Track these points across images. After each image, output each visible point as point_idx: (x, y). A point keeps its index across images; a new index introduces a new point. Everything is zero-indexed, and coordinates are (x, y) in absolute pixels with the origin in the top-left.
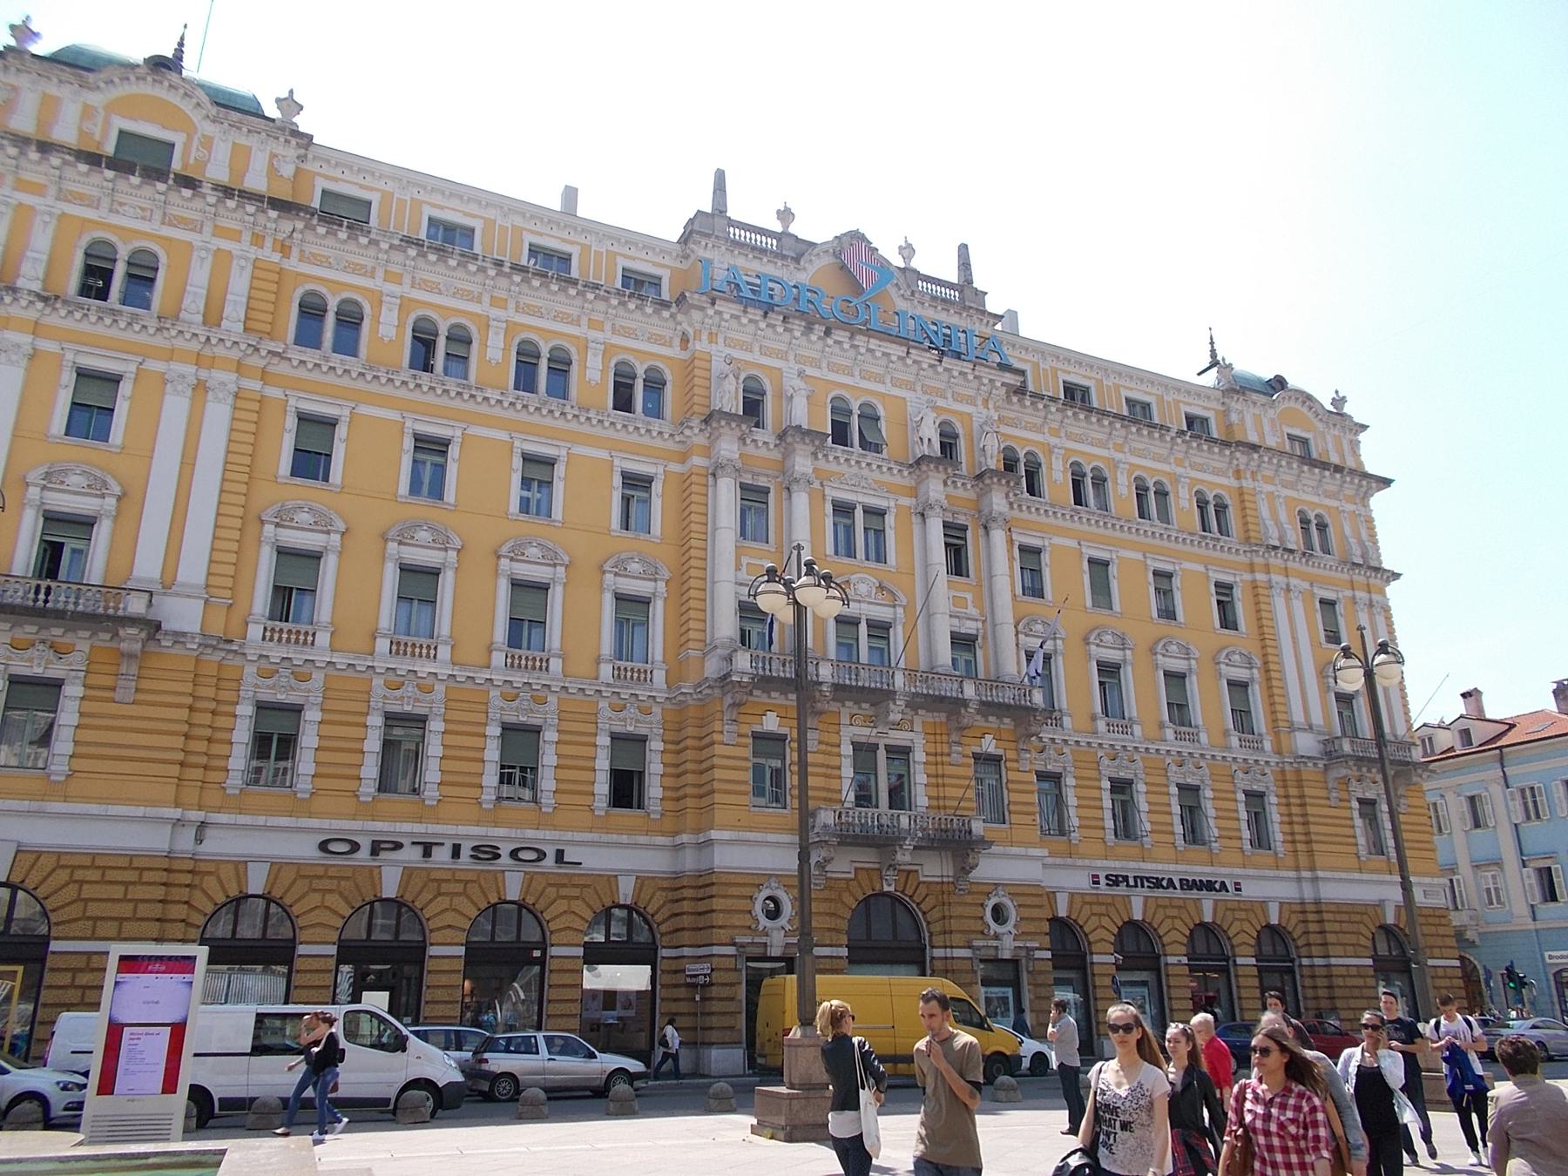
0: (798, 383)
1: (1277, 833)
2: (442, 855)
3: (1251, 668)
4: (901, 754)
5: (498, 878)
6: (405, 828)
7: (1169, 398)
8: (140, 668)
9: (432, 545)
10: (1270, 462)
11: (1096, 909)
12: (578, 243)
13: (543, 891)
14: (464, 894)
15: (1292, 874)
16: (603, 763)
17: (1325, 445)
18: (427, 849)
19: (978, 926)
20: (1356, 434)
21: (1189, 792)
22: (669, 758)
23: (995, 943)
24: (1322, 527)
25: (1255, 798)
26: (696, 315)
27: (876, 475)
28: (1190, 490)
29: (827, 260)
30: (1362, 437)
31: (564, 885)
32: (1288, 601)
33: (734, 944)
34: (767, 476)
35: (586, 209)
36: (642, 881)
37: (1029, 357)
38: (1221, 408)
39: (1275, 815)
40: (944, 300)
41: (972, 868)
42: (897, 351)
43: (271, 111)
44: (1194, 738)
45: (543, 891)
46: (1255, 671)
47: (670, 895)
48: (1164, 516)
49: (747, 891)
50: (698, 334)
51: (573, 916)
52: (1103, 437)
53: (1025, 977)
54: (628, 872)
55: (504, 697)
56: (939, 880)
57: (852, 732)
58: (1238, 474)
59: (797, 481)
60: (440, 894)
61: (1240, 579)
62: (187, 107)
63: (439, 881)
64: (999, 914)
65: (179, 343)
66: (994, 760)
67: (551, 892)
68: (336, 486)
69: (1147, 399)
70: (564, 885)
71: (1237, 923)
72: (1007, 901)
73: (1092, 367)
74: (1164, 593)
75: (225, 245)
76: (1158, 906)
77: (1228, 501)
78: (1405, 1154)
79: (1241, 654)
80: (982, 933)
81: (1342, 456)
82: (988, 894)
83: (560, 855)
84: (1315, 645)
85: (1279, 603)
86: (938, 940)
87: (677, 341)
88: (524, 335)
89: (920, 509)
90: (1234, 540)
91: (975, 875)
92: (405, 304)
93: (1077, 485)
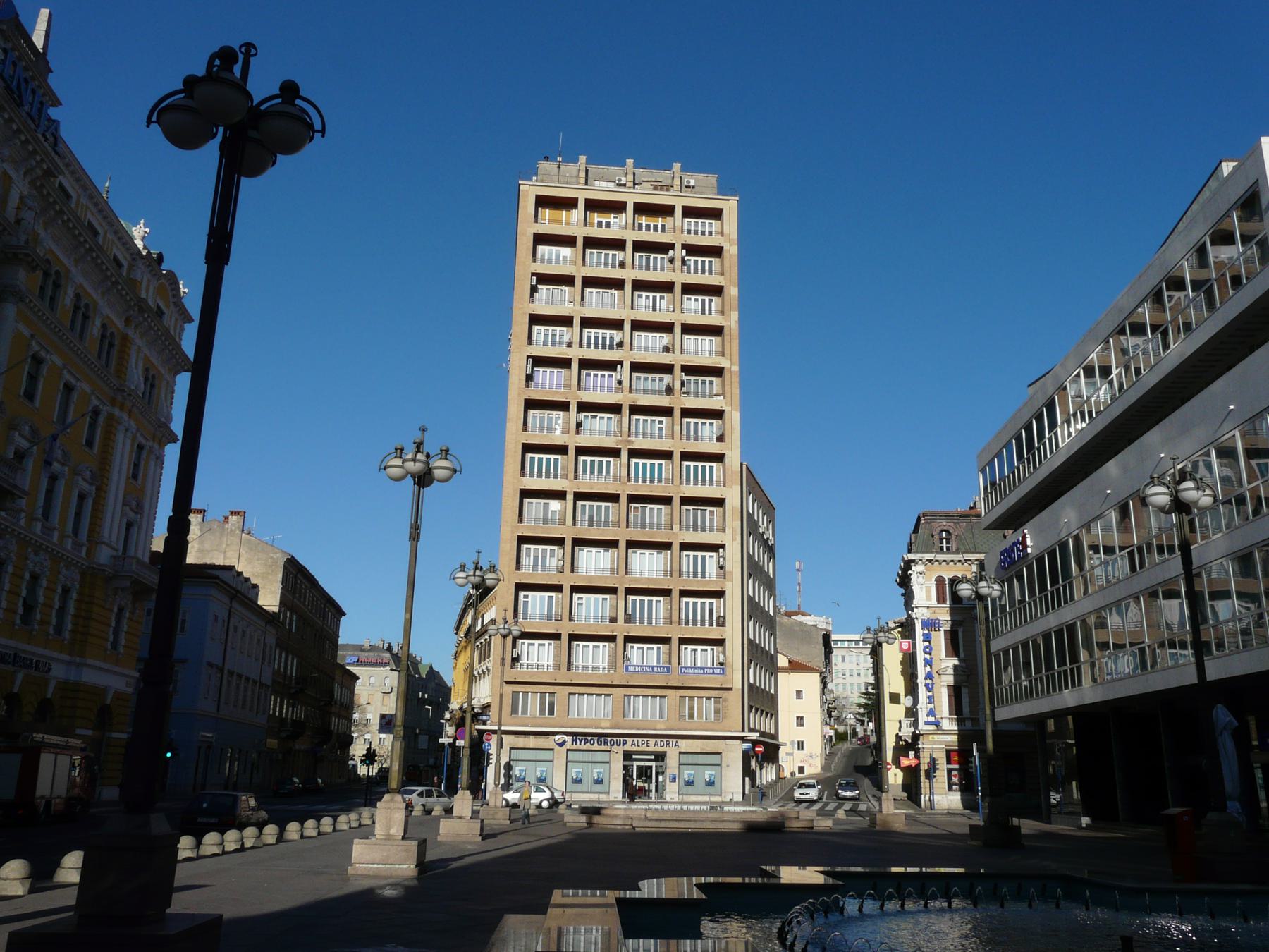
15: (66, 657)
20: (185, 323)
81: (147, 296)
85: (120, 437)
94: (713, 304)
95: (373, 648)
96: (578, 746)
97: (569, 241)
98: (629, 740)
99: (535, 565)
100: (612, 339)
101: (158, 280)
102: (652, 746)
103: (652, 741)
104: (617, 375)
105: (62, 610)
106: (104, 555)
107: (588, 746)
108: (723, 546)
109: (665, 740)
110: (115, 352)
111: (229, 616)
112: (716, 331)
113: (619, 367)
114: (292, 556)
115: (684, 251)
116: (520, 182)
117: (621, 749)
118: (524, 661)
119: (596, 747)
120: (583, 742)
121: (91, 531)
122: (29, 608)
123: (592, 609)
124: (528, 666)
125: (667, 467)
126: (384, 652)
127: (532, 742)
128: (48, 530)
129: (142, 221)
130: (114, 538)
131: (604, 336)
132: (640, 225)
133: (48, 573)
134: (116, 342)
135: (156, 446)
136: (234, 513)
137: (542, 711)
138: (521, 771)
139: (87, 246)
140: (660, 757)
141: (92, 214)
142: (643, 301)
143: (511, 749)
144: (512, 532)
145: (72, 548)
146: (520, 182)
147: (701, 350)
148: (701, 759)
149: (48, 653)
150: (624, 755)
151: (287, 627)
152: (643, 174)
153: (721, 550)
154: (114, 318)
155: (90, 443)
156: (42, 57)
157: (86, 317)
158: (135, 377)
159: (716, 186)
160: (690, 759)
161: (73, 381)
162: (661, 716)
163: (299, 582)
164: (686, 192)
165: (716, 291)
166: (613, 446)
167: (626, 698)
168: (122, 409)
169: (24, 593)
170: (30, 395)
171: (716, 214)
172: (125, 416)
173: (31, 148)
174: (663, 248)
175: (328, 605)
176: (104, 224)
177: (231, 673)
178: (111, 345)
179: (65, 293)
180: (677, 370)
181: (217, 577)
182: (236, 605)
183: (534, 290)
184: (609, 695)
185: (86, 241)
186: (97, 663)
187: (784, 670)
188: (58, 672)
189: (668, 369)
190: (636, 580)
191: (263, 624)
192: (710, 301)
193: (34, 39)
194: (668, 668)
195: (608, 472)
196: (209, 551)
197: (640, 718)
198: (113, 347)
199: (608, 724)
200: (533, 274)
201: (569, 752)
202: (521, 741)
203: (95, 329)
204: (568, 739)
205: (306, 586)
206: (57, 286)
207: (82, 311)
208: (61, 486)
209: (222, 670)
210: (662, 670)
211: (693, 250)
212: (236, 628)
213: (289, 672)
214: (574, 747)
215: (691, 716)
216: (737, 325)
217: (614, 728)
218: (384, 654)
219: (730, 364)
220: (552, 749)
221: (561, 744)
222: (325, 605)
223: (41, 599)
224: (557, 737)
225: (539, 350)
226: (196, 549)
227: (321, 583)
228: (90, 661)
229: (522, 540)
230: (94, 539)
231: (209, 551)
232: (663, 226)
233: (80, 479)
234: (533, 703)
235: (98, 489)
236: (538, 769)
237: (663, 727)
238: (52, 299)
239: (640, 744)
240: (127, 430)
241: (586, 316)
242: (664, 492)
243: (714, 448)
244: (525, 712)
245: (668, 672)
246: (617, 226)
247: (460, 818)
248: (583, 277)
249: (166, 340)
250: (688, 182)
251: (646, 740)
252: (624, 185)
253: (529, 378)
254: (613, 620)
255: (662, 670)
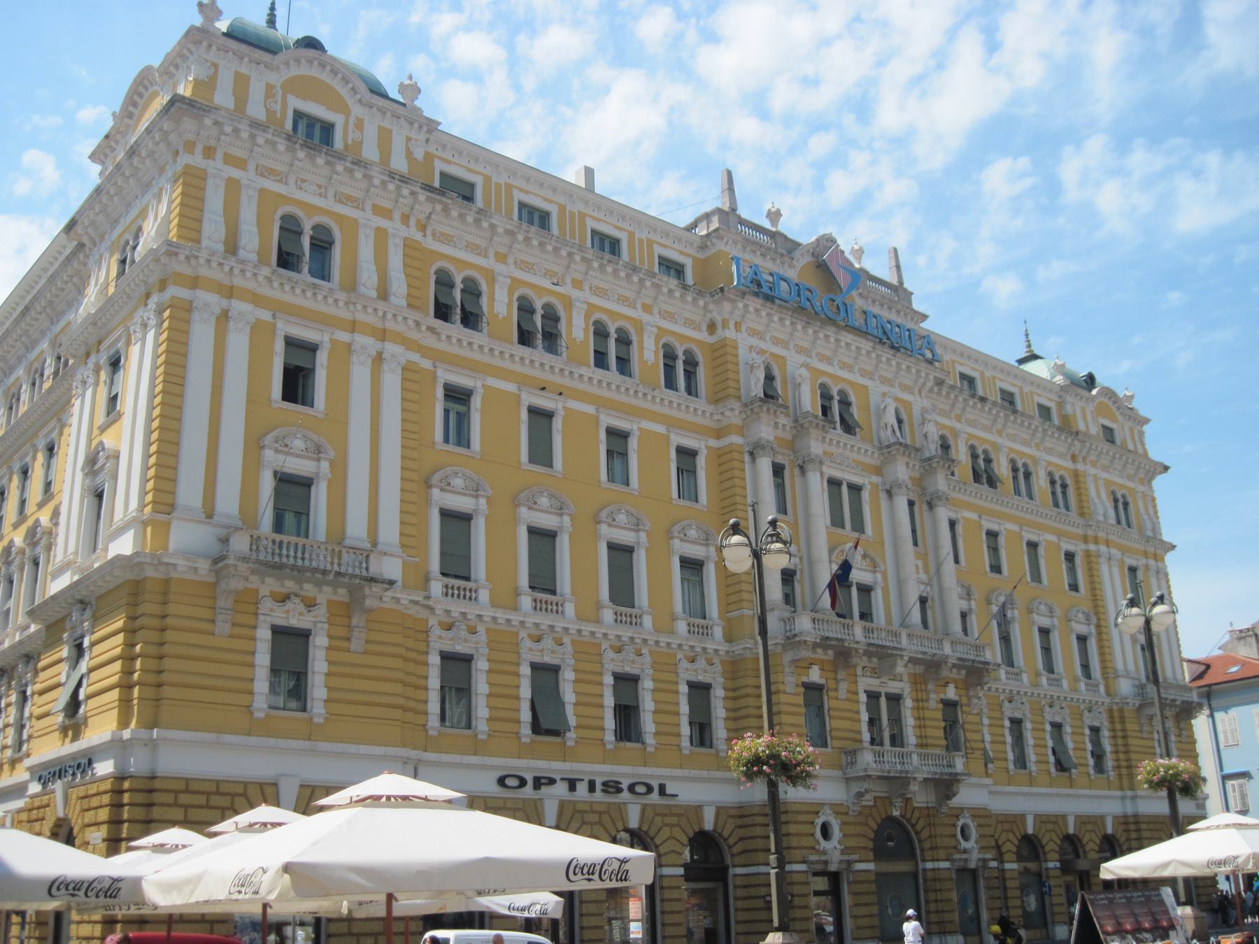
0: (804, 372)
2: (582, 788)
3: (1052, 617)
4: (895, 699)
5: (621, 809)
6: (556, 767)
7: (1027, 389)
8: (368, 620)
9: (550, 509)
10: (1120, 458)
11: (668, 820)
12: (556, 203)
13: (653, 820)
14: (600, 823)
15: (1119, 793)
16: (609, 701)
17: (1122, 432)
18: (572, 784)
19: (952, 843)
20: (1142, 426)
21: (626, 682)
22: (730, 704)
23: (965, 856)
24: (1126, 505)
25: (699, 691)
26: (727, 306)
27: (854, 456)
28: (587, 316)
29: (808, 259)
30: (1146, 428)
31: (666, 815)
32: (1110, 567)
33: (804, 862)
35: (602, 186)
36: (720, 810)
37: (479, 168)
38: (1058, 400)
40: (754, 243)
41: (954, 795)
42: (866, 345)
43: (394, 93)
44: (634, 621)
45: (653, 820)
46: (1055, 620)
47: (739, 821)
49: (809, 817)
50: (725, 324)
51: (674, 841)
52: (947, 408)
53: (845, 888)
54: (709, 804)
55: (441, 624)
56: (925, 805)
58: (1074, 458)
59: (812, 461)
60: (584, 823)
62: (344, 92)
63: (582, 812)
64: (826, 831)
65: (360, 316)
67: (658, 820)
68: (559, 472)
70: (666, 815)
71: (1087, 834)
72: (969, 822)
74: (994, 550)
75: (236, 173)
76: (1003, 831)
77: (700, 358)
80: (813, 848)
83: (662, 788)
84: (254, 398)
85: (1104, 568)
86: (928, 855)
87: (704, 327)
88: (440, 264)
89: (888, 487)
90: (1134, 532)
91: (956, 801)
93: (669, 369)
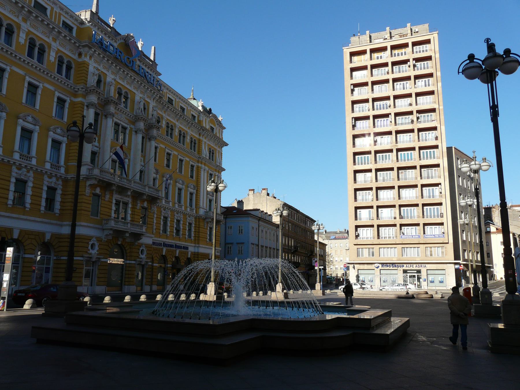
1: (57, 206)
15: (194, 245)
20: (223, 130)
30: (224, 130)
34: (100, 110)
39: (58, 198)
48: (40, 60)
57: (116, 196)
58: (200, 135)
61: (195, 165)
66: (98, 196)
69: (184, 107)
72: (144, 249)
73: (189, 105)
78: (463, 280)
79: (32, 117)
81: (206, 126)
82: (140, 246)
85: (202, 172)
92: (29, 33)
94: (430, 81)
95: (341, 232)
96: (384, 268)
97: (365, 68)
98: (405, 265)
99: (363, 199)
100: (386, 104)
101: (209, 118)
102: (415, 267)
103: (415, 265)
104: (389, 119)
105: (190, 230)
106: (202, 212)
107: (388, 268)
108: (440, 184)
109: (420, 265)
110: (197, 145)
111: (259, 227)
112: (432, 93)
113: (390, 115)
114: (285, 203)
115: (414, 61)
116: (343, 48)
117: (402, 269)
118: (361, 236)
119: (391, 268)
120: (386, 266)
121: (196, 204)
122: (178, 231)
123: (386, 215)
124: (385, 237)
125: (414, 154)
126: (345, 234)
127: (366, 267)
128: (180, 206)
129: (201, 100)
130: (205, 205)
131: (377, 104)
132: (395, 54)
133: (182, 219)
134: (197, 142)
135: (217, 174)
136: (263, 189)
137: (369, 255)
138: (363, 278)
139: (179, 115)
140: (419, 271)
141: (181, 103)
142: (398, 86)
143: (358, 270)
144: (352, 187)
145: (190, 210)
146: (343, 48)
147: (425, 102)
148: (437, 272)
149: (186, 244)
150: (403, 271)
151: (287, 228)
152: (394, 32)
153: (440, 186)
154: (195, 135)
155: (192, 177)
156: (154, 62)
157: (184, 137)
158: (205, 153)
159: (428, 29)
160: (432, 272)
161: (182, 158)
162: (418, 255)
163: (293, 213)
164: (416, 35)
165: (431, 75)
166: (390, 148)
167: (403, 249)
168: (201, 164)
169: (175, 226)
170: (168, 166)
171: (428, 42)
172: (203, 166)
173: (153, 92)
174: (405, 62)
175: (306, 218)
176: (186, 105)
177: (262, 246)
178: (195, 143)
179: (175, 131)
180: (415, 112)
181: (251, 214)
182: (260, 222)
183: (353, 91)
184: (396, 248)
185: (178, 113)
186: (204, 246)
187: (494, 233)
188: (191, 249)
189: (411, 113)
190: (403, 201)
191: (276, 228)
192: (429, 80)
193: (151, 58)
194: (419, 236)
195: (389, 159)
196: (257, 204)
197: (409, 256)
198: (195, 144)
199: (396, 259)
200: (351, 85)
201: (428, 271)
202: (362, 267)
203: (188, 140)
204: (380, 265)
205: (294, 213)
206: (172, 129)
207: (182, 136)
208: (183, 192)
209: (258, 245)
210: (416, 237)
211: (418, 60)
212: (262, 231)
213: (290, 244)
214: (383, 268)
215: (431, 255)
216: (441, 89)
217: (398, 261)
218: (345, 235)
219: (440, 107)
220: (374, 269)
221: (377, 268)
222: (305, 219)
223: (182, 228)
224: (375, 265)
225: (357, 114)
226: (252, 204)
227: (301, 211)
228: (201, 246)
229: (356, 190)
230: (197, 207)
231: (257, 204)
232: (405, 52)
233: (189, 188)
234: (366, 252)
235: (197, 191)
236: (369, 277)
237: (419, 259)
238: (171, 134)
239: (409, 267)
240: (204, 170)
241: (374, 97)
242: (412, 164)
243: (434, 143)
244: (362, 255)
245: (419, 237)
246: (386, 57)
247: (279, 292)
248: (371, 81)
249: (215, 137)
250: (415, 30)
251: (412, 265)
252: (386, 39)
253: (354, 126)
254: (395, 218)
255: (416, 237)
